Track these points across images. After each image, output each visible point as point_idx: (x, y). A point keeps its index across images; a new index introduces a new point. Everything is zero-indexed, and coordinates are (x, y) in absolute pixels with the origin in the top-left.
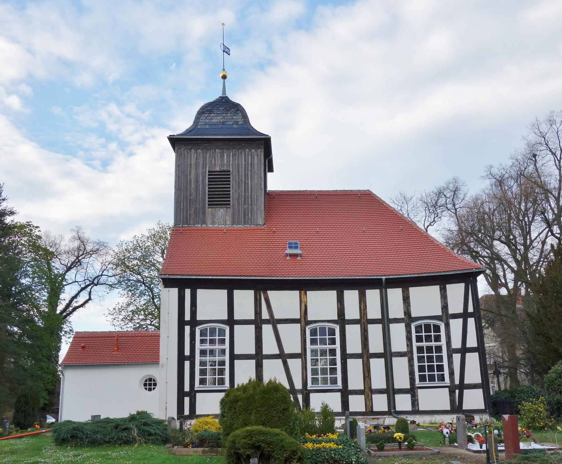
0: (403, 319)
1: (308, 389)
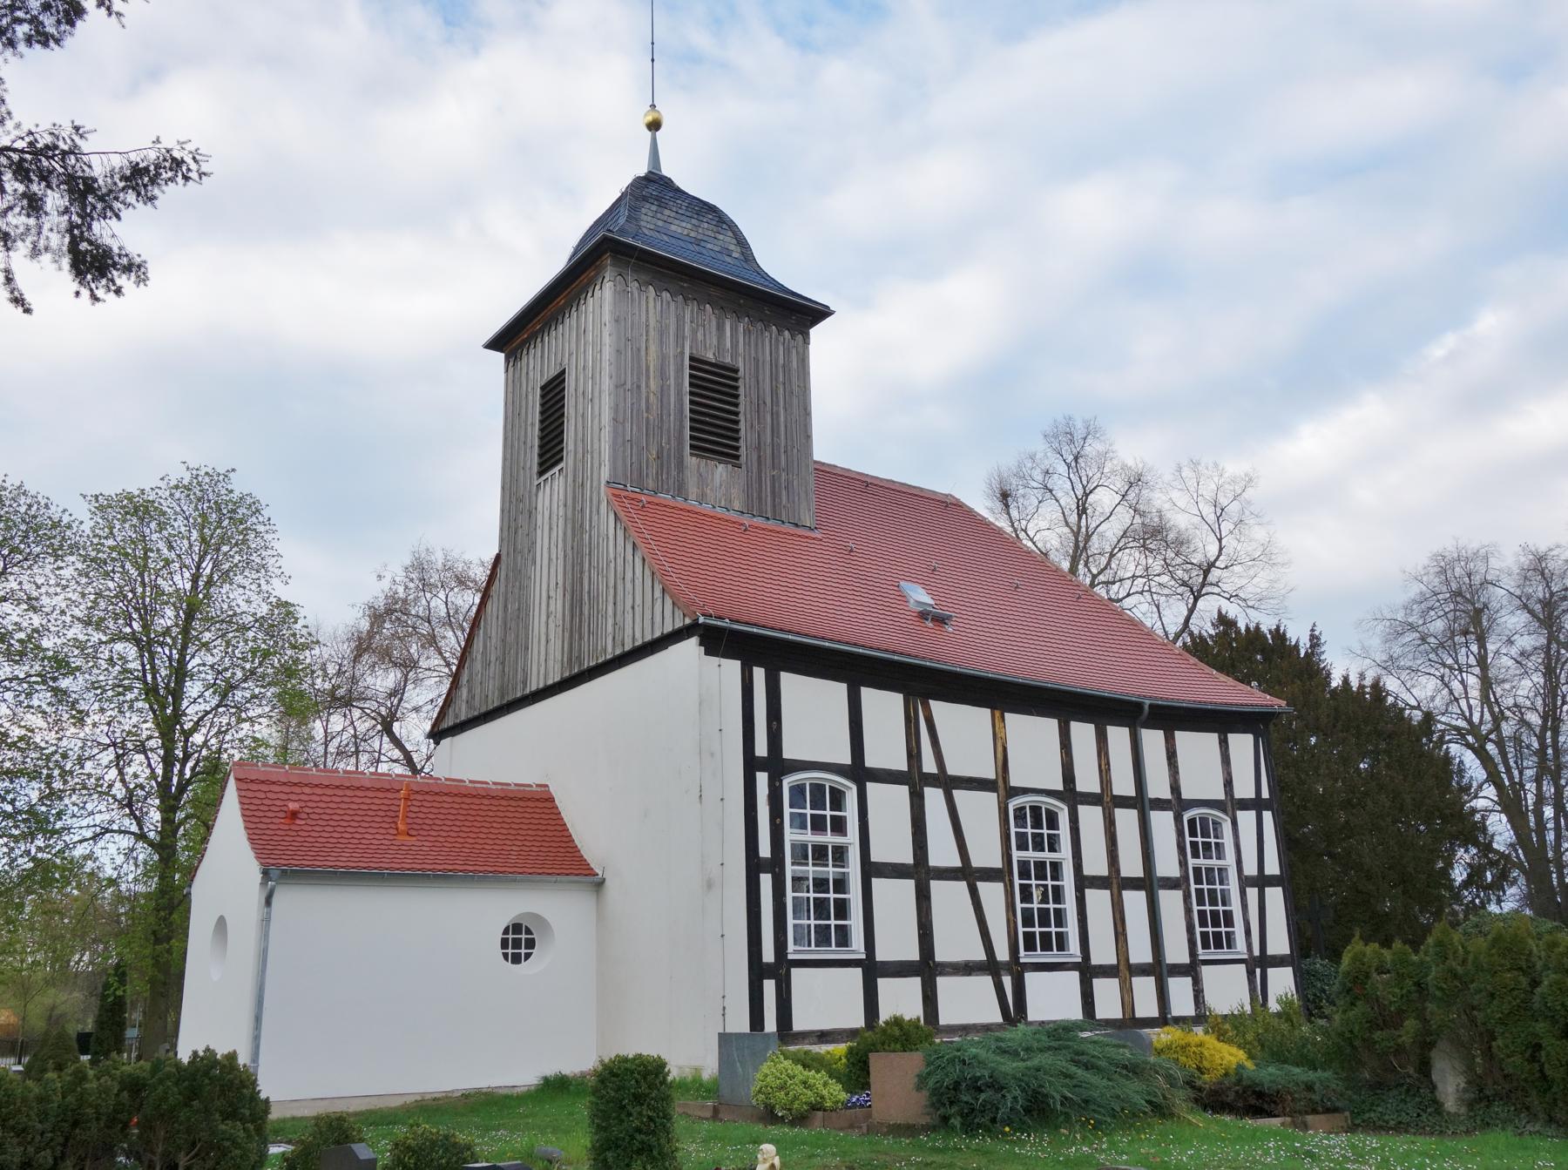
0: (1168, 801)
1: (1022, 961)
